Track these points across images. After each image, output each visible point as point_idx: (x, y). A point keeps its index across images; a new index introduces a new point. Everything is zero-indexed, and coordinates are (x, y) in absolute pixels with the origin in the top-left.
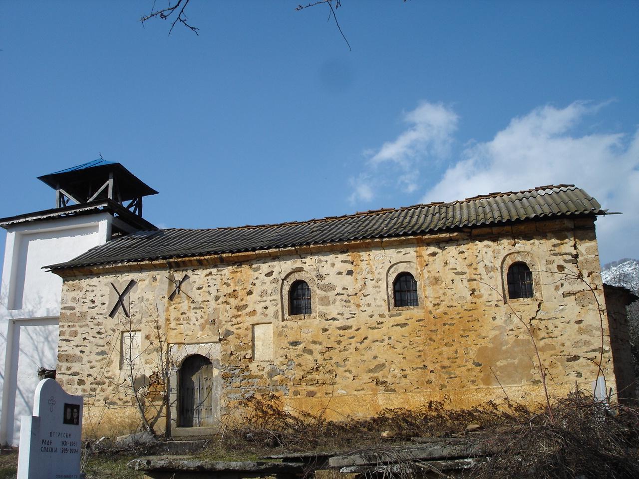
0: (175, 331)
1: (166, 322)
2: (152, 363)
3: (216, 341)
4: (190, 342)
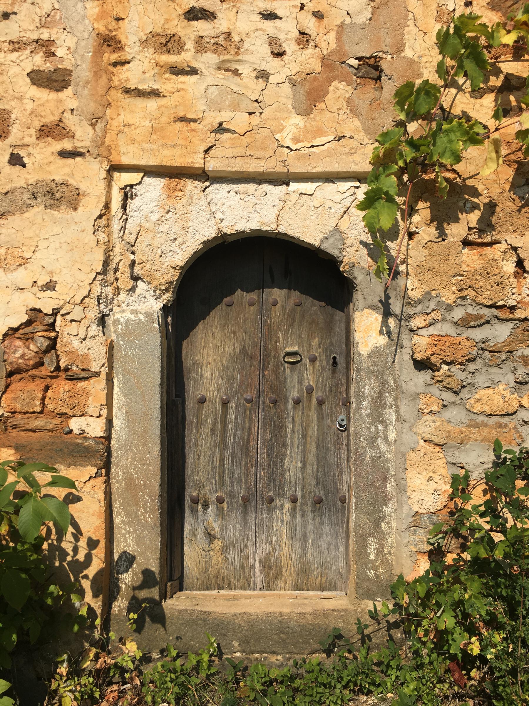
0: (152, 104)
1: (98, 52)
2: (23, 262)
3: (354, 168)
4: (238, 166)
